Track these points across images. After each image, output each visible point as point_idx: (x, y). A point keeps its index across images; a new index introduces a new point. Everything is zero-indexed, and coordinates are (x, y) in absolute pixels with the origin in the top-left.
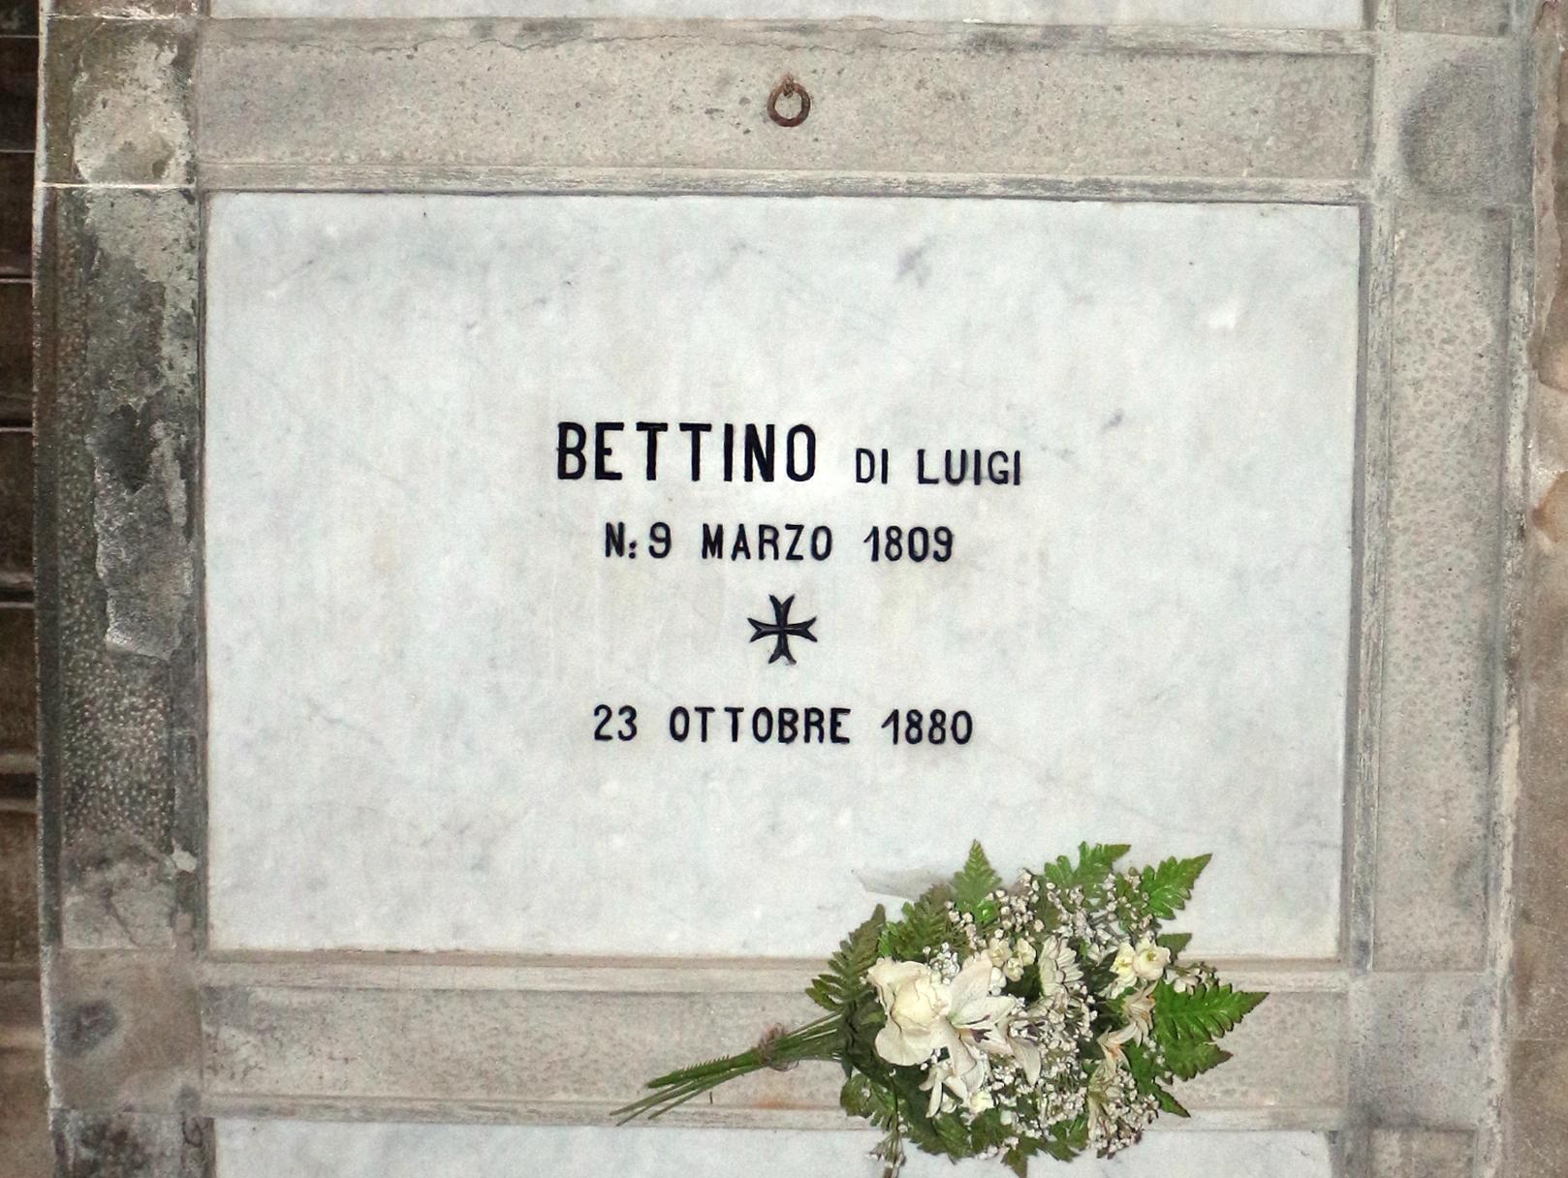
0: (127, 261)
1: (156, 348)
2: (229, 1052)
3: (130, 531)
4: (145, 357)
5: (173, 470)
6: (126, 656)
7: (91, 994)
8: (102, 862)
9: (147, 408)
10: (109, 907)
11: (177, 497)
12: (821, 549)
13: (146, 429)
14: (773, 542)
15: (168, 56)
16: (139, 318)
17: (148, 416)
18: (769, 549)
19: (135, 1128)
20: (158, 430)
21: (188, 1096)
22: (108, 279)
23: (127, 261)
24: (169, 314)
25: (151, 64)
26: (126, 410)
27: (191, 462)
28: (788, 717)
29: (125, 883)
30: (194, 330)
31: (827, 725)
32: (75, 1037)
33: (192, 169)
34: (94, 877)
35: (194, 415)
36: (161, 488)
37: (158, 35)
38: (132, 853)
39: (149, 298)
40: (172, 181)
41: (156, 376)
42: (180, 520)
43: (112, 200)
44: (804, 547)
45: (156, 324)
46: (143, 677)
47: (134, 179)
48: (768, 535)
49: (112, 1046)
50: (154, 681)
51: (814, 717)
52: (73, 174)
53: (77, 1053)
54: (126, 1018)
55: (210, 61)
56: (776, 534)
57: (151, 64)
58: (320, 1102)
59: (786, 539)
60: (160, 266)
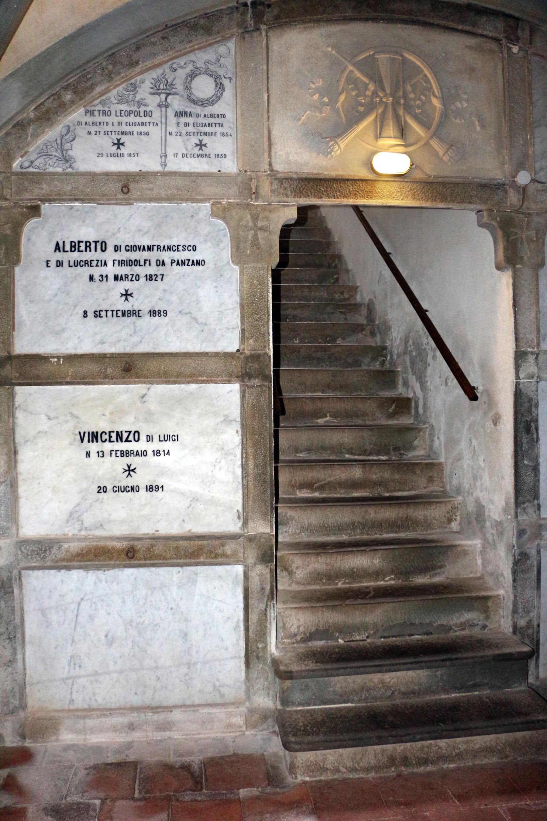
0: (526, 394)
1: (531, 409)
2: (544, 536)
3: (527, 442)
4: (530, 412)
5: (534, 431)
6: (527, 465)
7: (522, 528)
8: (524, 503)
9: (530, 421)
10: (525, 511)
11: (535, 436)
12: (137, 279)
13: (530, 424)
14: (127, 278)
15: (534, 357)
16: (529, 404)
17: (530, 422)
18: (127, 279)
19: (528, 552)
20: (532, 424)
21: (538, 545)
22: (523, 397)
23: (526, 394)
24: (533, 403)
25: (531, 358)
26: (527, 421)
27: (537, 429)
28: (134, 312)
29: (527, 506)
30: (537, 406)
31: (137, 314)
32: (520, 536)
33: (538, 377)
34: (522, 506)
35: (537, 421)
36: (532, 435)
37: (532, 353)
38: (529, 501)
39: (530, 400)
40: (535, 379)
41: (531, 414)
42: (535, 440)
43: (524, 383)
44: (134, 279)
45: (531, 405)
46: (530, 469)
47: (528, 379)
48: (127, 276)
49: (525, 537)
50: (532, 469)
51: (134, 312)
52: (519, 379)
53: (520, 539)
54: (528, 531)
55: (541, 357)
56: (128, 276)
57: (531, 358)
58: (414, 501)
59: (130, 277)
60: (531, 394)
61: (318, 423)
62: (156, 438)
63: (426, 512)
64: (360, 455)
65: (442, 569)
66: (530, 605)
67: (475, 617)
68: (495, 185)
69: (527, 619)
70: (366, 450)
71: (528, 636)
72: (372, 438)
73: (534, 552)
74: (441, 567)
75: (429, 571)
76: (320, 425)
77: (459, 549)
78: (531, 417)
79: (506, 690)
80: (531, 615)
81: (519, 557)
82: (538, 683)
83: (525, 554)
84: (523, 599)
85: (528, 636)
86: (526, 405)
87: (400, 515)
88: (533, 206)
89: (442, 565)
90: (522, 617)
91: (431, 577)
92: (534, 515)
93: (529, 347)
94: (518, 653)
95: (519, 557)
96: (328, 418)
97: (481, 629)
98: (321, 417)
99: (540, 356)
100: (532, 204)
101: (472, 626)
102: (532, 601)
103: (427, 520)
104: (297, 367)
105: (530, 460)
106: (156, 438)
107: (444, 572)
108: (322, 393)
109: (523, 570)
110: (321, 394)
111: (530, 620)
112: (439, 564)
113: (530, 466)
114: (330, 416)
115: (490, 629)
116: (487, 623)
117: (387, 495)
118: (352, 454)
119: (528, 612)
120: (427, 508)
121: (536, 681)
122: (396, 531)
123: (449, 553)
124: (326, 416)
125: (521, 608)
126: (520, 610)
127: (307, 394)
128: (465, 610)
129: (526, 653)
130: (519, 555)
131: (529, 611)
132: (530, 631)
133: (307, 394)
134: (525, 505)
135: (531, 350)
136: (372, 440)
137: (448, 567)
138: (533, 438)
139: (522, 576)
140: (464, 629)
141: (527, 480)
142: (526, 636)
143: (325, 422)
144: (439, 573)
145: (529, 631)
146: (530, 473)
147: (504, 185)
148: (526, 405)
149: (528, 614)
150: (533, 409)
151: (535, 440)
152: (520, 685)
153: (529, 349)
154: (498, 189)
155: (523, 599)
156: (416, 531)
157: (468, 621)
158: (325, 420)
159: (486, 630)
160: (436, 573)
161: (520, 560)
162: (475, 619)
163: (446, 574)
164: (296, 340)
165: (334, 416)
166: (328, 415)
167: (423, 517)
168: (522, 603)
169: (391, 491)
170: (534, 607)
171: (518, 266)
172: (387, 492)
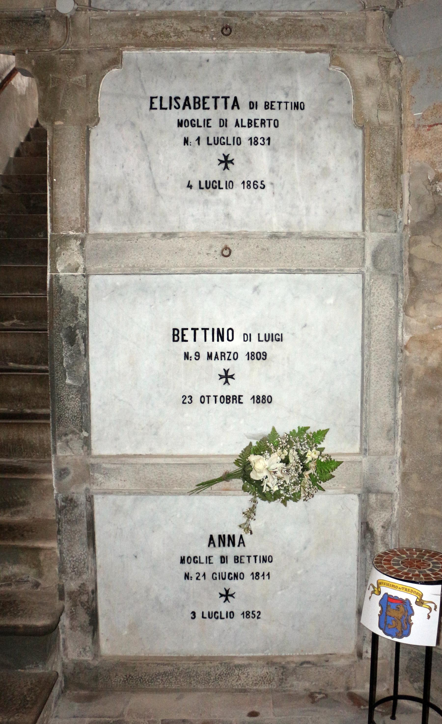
0: (70, 291)
1: (77, 312)
2: (96, 479)
4: (74, 314)
5: (81, 341)
7: (64, 466)
8: (66, 435)
9: (75, 326)
10: (68, 445)
11: (82, 347)
15: (79, 243)
19: (75, 498)
20: (78, 331)
21: (87, 490)
22: (65, 296)
23: (70, 291)
24: (80, 304)
26: (70, 327)
27: (85, 339)
30: (86, 308)
32: (60, 476)
33: (85, 270)
34: (64, 438)
35: (86, 328)
36: (79, 345)
37: (76, 238)
38: (73, 432)
39: (75, 300)
40: (80, 272)
41: (77, 319)
42: (83, 353)
43: (66, 277)
46: (75, 390)
49: (68, 478)
52: (56, 271)
53: (61, 480)
54: (72, 471)
55: (89, 244)
57: (74, 245)
60: (77, 293)
61: (3, 326)
62: (254, 337)
63: (41, 436)
64: (26, 363)
65: (25, 507)
66: (82, 565)
67: (23, 572)
68: (31, 18)
69: (80, 582)
70: (32, 358)
71: (82, 603)
72: (40, 345)
73: (82, 499)
74: (24, 504)
75: (9, 507)
76: (4, 327)
77: (45, 484)
78: (75, 322)
79: (19, 670)
80: (85, 577)
81: (63, 504)
82: (96, 663)
83: (71, 500)
84: (72, 556)
85: (82, 603)
86: (70, 306)
87: (11, 437)
88: (83, 42)
89: (24, 502)
90: (71, 578)
91: (13, 514)
92: (82, 451)
93: (72, 229)
94: (25, 627)
95: (63, 504)
96: (15, 321)
97: (33, 587)
98: (6, 320)
99: (87, 242)
100: (81, 39)
101: (20, 582)
102: (84, 560)
103: (44, 444)
104: (23, 264)
105: (74, 378)
106: (254, 337)
107: (27, 511)
108: (31, 293)
109: (70, 521)
110: (29, 294)
111: (83, 584)
112: (21, 500)
113: (75, 387)
114: (18, 319)
115: (44, 588)
116: (40, 581)
117: (29, 411)
118: (15, 362)
119: (80, 574)
120: (43, 431)
121: (94, 659)
122: (7, 456)
123: (33, 488)
124: (13, 319)
125: (70, 567)
126: (69, 570)
127: (14, 294)
128: (9, 562)
129: (45, 627)
130: (63, 501)
131: (80, 573)
132: (84, 598)
133: (14, 294)
134: (69, 437)
135: (75, 233)
136: (40, 347)
137: (32, 505)
138: (79, 350)
139: (69, 527)
140: (10, 585)
141: (69, 404)
142: (78, 603)
143: (11, 325)
144: (22, 511)
145: (82, 598)
146: (74, 396)
147: (44, 16)
148: (70, 306)
149: (80, 575)
150: (80, 312)
151: (83, 353)
152: (37, 666)
153: (71, 233)
154: (37, 22)
155: (72, 556)
156: (31, 457)
157: (15, 575)
158: (11, 322)
159: (39, 590)
160: (18, 511)
161: (65, 507)
162: (23, 574)
163: (31, 513)
164: (40, 234)
165: (22, 319)
166: (15, 317)
167: (38, 441)
168: (70, 561)
169: (34, 407)
170: (88, 568)
171: (57, 123)
172: (29, 408)
